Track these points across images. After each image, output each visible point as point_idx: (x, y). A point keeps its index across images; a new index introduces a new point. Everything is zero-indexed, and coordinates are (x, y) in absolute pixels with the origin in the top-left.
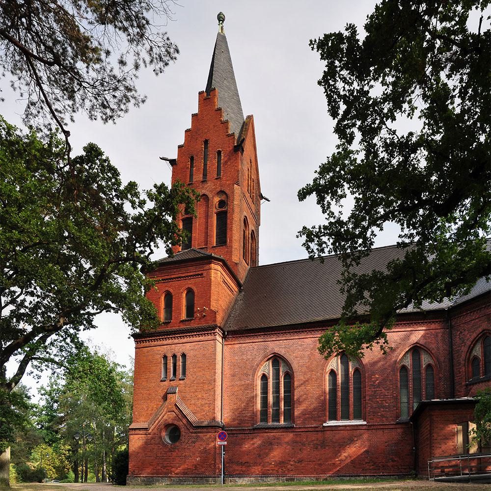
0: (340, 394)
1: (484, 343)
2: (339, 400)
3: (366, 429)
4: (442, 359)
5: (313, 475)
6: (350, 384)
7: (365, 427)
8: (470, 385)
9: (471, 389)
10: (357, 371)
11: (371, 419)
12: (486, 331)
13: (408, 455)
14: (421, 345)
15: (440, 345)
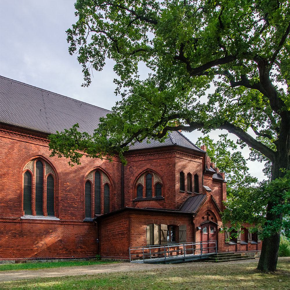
0: (35, 192)
1: (146, 177)
2: (34, 196)
3: (59, 224)
4: (116, 182)
5: (11, 259)
6: (45, 185)
7: (58, 223)
8: (136, 201)
9: (137, 204)
10: (50, 176)
11: (63, 217)
12: (149, 170)
13: (93, 244)
14: (103, 169)
15: (116, 172)
